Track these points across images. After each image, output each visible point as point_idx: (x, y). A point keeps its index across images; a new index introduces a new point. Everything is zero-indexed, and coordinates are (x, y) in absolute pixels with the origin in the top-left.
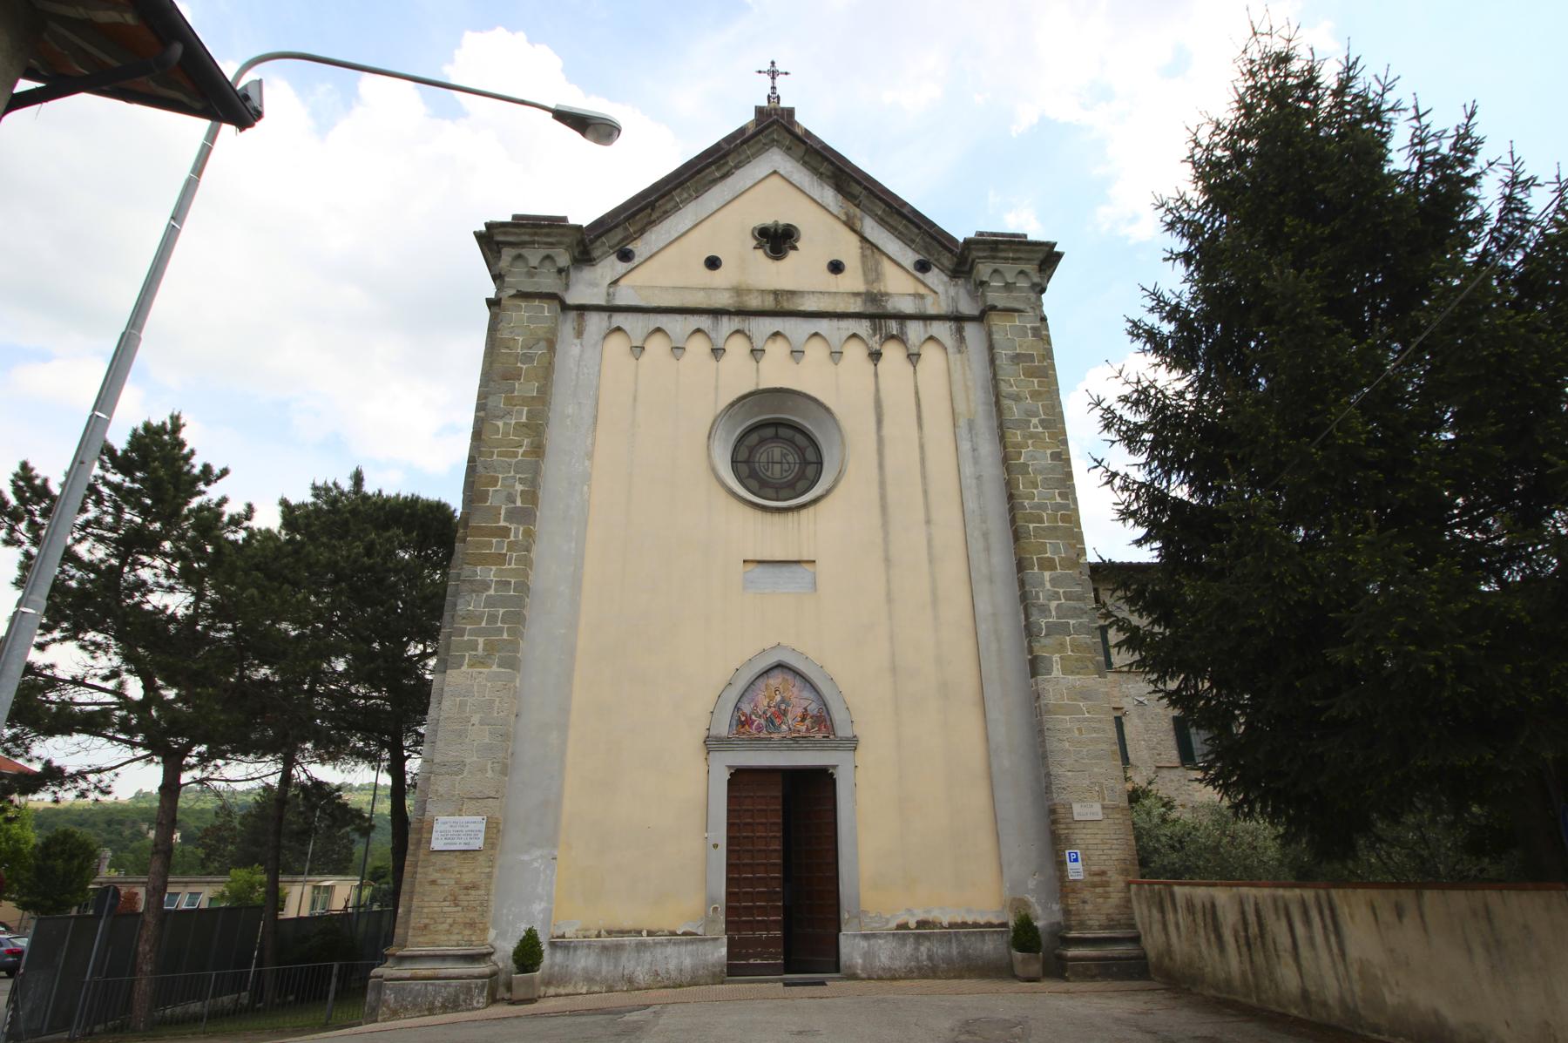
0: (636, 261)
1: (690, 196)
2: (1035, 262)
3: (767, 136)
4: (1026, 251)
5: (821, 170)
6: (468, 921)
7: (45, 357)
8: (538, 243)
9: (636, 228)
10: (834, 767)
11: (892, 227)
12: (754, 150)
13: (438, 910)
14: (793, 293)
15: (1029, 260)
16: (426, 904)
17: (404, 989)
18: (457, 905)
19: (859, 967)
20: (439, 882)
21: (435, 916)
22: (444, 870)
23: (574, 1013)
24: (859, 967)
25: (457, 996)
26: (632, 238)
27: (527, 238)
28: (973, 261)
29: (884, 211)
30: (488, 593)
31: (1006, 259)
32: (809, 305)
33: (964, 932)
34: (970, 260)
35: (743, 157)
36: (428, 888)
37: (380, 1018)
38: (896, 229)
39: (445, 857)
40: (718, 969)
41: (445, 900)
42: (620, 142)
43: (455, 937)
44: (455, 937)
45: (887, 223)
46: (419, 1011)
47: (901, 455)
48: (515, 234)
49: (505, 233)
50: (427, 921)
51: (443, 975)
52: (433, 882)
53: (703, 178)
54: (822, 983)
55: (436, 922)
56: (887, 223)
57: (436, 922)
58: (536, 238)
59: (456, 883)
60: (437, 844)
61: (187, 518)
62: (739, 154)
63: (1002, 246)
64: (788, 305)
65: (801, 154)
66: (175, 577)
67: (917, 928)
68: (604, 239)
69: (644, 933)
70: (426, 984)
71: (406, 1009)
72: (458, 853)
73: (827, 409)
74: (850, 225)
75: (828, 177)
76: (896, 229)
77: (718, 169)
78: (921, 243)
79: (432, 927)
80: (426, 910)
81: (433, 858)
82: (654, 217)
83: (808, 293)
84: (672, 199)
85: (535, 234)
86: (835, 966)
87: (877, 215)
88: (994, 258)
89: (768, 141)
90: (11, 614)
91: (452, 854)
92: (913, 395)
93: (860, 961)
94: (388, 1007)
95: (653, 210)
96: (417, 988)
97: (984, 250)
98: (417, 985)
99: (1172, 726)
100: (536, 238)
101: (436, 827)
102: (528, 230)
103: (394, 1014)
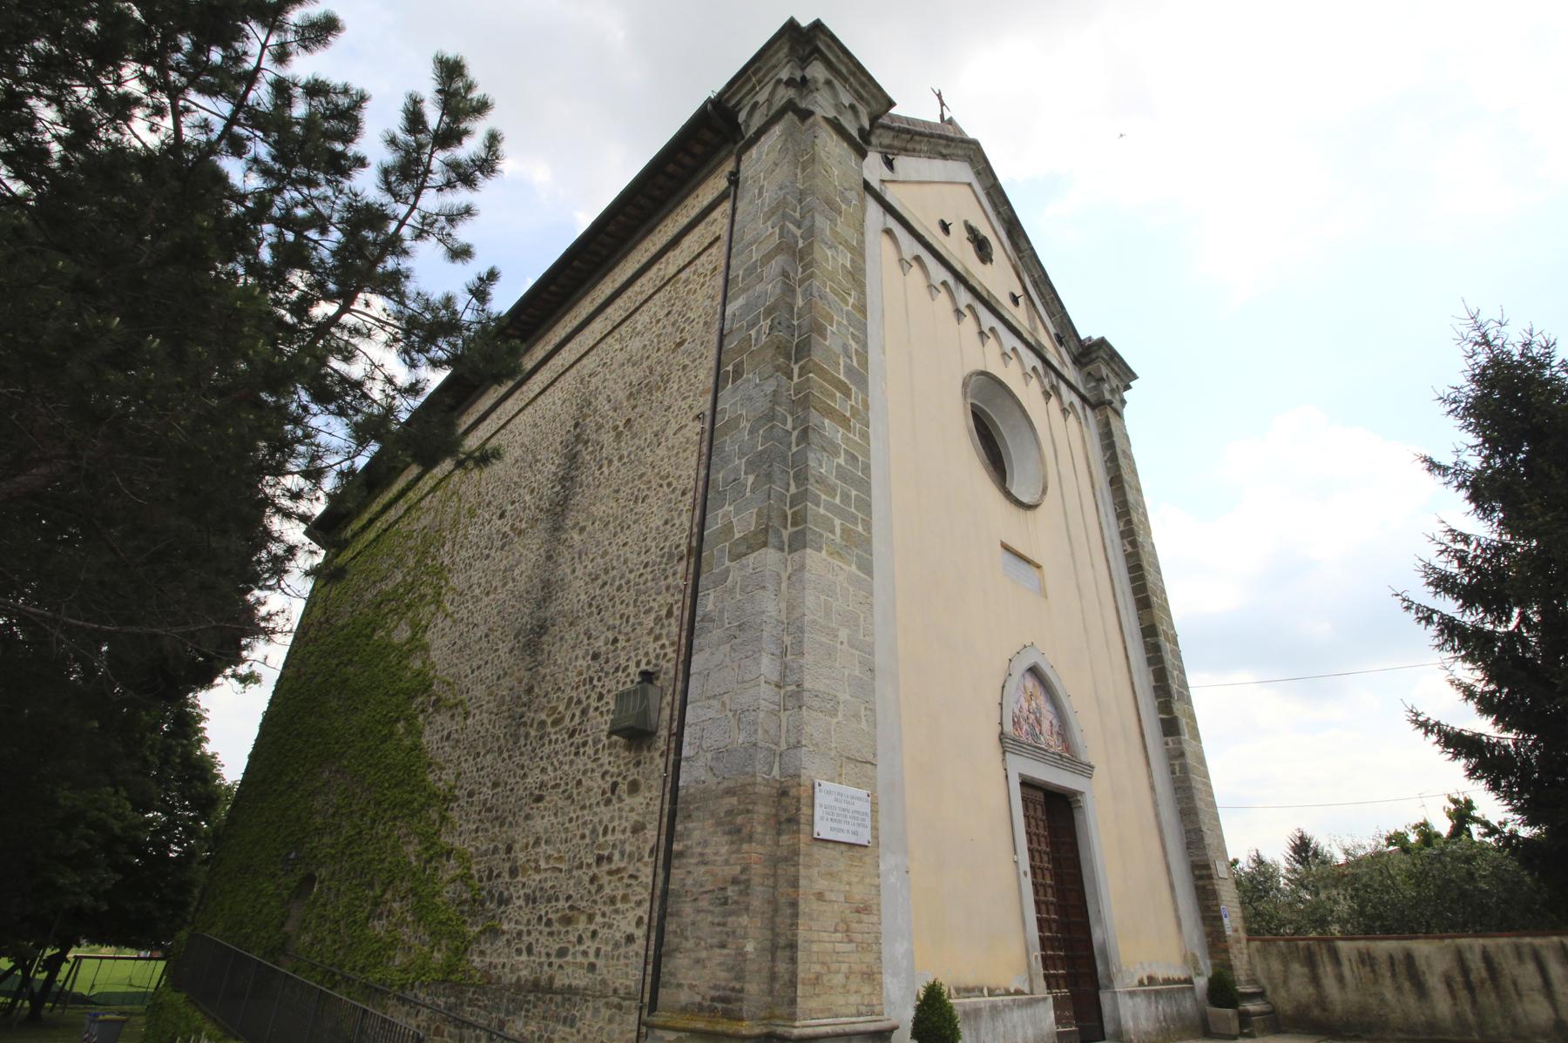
6: (865, 969)
8: (851, 85)
11: (1042, 294)
13: (829, 946)
18: (851, 941)
19: (1132, 1031)
22: (831, 874)
23: (643, 993)
24: (1132, 1031)
26: (905, 151)
27: (844, 71)
29: (1040, 276)
30: (843, 463)
33: (80, 620)
34: (1094, 356)
36: (815, 905)
38: (1044, 298)
39: (829, 852)
41: (836, 931)
43: (854, 999)
44: (854, 999)
45: (1037, 286)
48: (838, 57)
49: (829, 47)
55: (829, 971)
56: (1037, 286)
57: (829, 971)
58: (852, 79)
60: (823, 829)
65: (989, 185)
66: (61, 110)
67: (1163, 984)
72: (843, 848)
75: (1003, 219)
76: (1044, 298)
79: (825, 978)
80: (815, 947)
81: (820, 853)
85: (853, 74)
97: (1107, 355)
100: (852, 79)
101: (820, 798)
102: (850, 64)
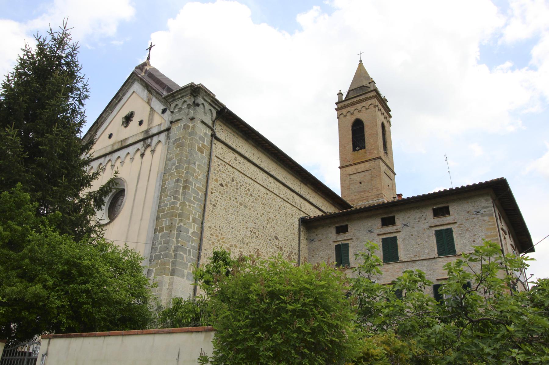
0: (162, 115)
1: (109, 113)
2: (189, 95)
3: (132, 79)
4: (184, 92)
7: (143, 145)
9: (93, 132)
12: (128, 87)
14: (126, 139)
15: (186, 95)
31: (179, 98)
32: (129, 142)
35: (125, 91)
53: (112, 105)
54: (438, 280)
61: (13, 230)
62: (123, 91)
63: (175, 94)
64: (124, 145)
68: (84, 140)
74: (149, 103)
77: (116, 99)
82: (98, 126)
83: (130, 137)
84: (103, 117)
88: (175, 100)
89: (132, 81)
90: (389, 104)
92: (137, 175)
95: (98, 124)
97: (171, 98)
99: (432, 291)
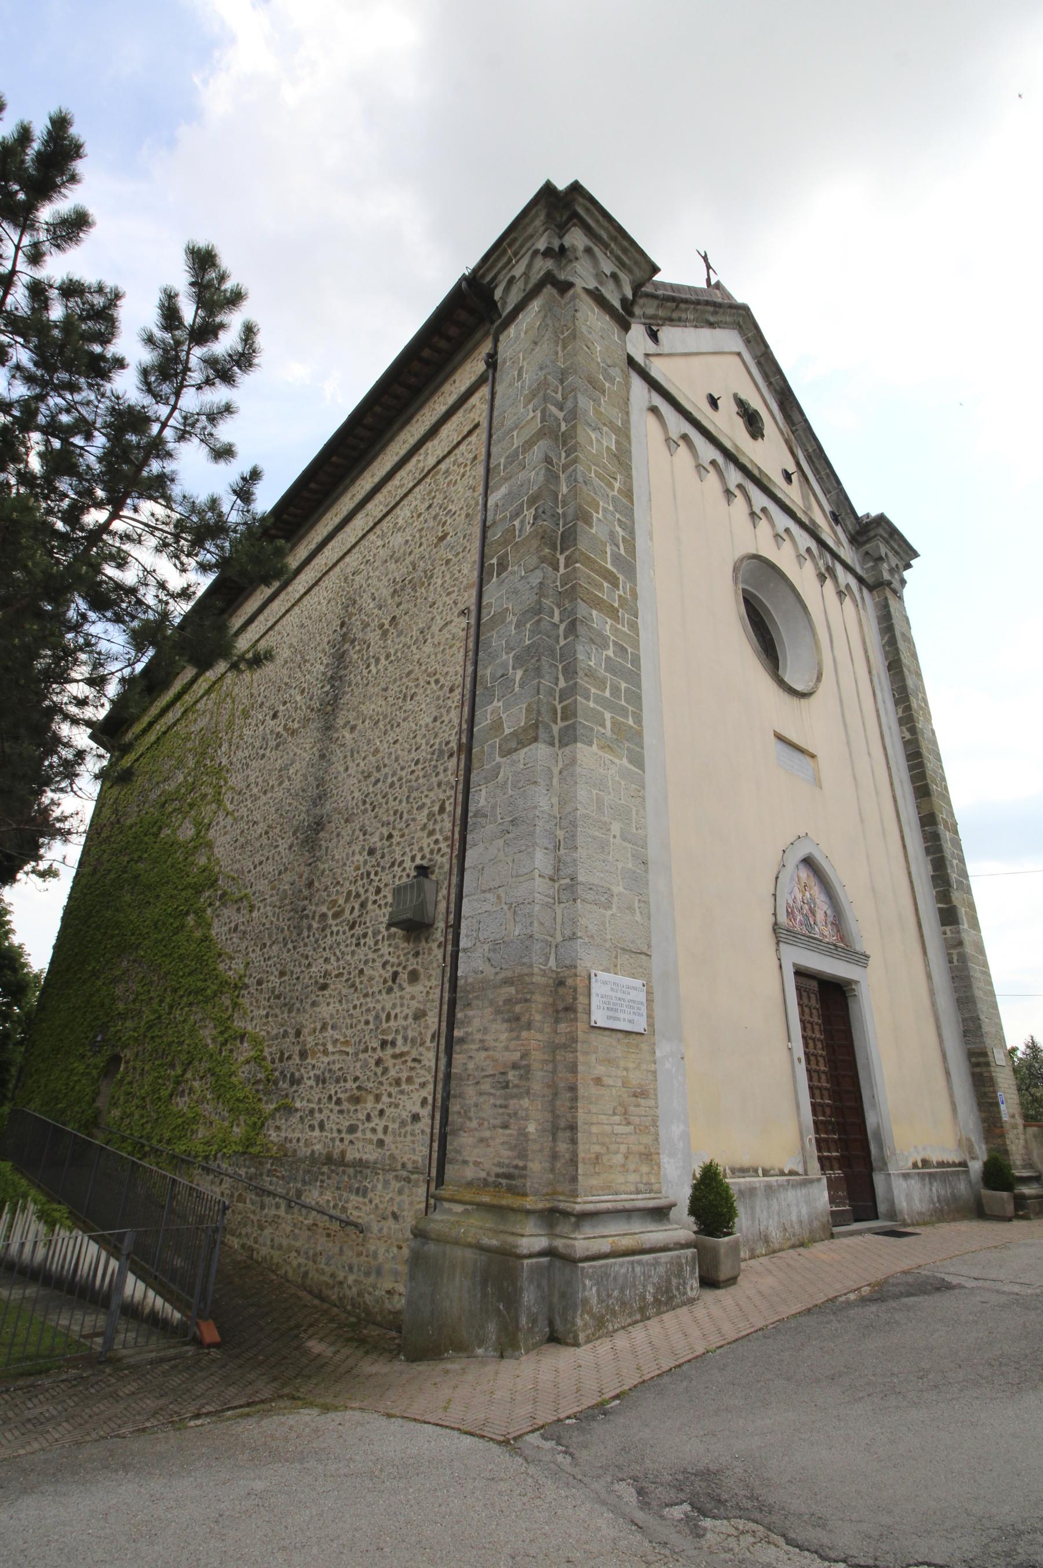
5: (772, 380)
6: (643, 1150)
10: (857, 982)
11: (817, 469)
13: (607, 1129)
16: (595, 1120)
17: (608, 1276)
18: (629, 1124)
20: (607, 1081)
21: (607, 1140)
22: (609, 1061)
25: (669, 1281)
26: (670, 321)
27: (605, 236)
28: (875, 536)
29: (814, 450)
37: (582, 1337)
39: (607, 1039)
40: (825, 1220)
41: (614, 1114)
42: (202, 243)
43: (633, 1177)
45: (812, 461)
46: (630, 1315)
47: (847, 682)
48: (597, 221)
49: (587, 210)
50: (597, 1148)
51: (647, 1246)
52: (598, 1081)
56: (812, 461)
58: (613, 245)
59: (624, 1085)
60: (599, 1018)
69: (760, 1172)
70: (633, 1262)
71: (614, 1313)
72: (620, 1035)
73: (804, 607)
75: (776, 391)
78: (835, 497)
79: (605, 1158)
80: (594, 1129)
81: (595, 1038)
86: (668, 1219)
87: (807, 450)
91: (614, 1034)
93: (905, 1204)
94: (590, 1312)
96: (623, 1271)
98: (622, 1265)
100: (613, 245)
101: (596, 988)
102: (611, 228)
103: (601, 1326)
